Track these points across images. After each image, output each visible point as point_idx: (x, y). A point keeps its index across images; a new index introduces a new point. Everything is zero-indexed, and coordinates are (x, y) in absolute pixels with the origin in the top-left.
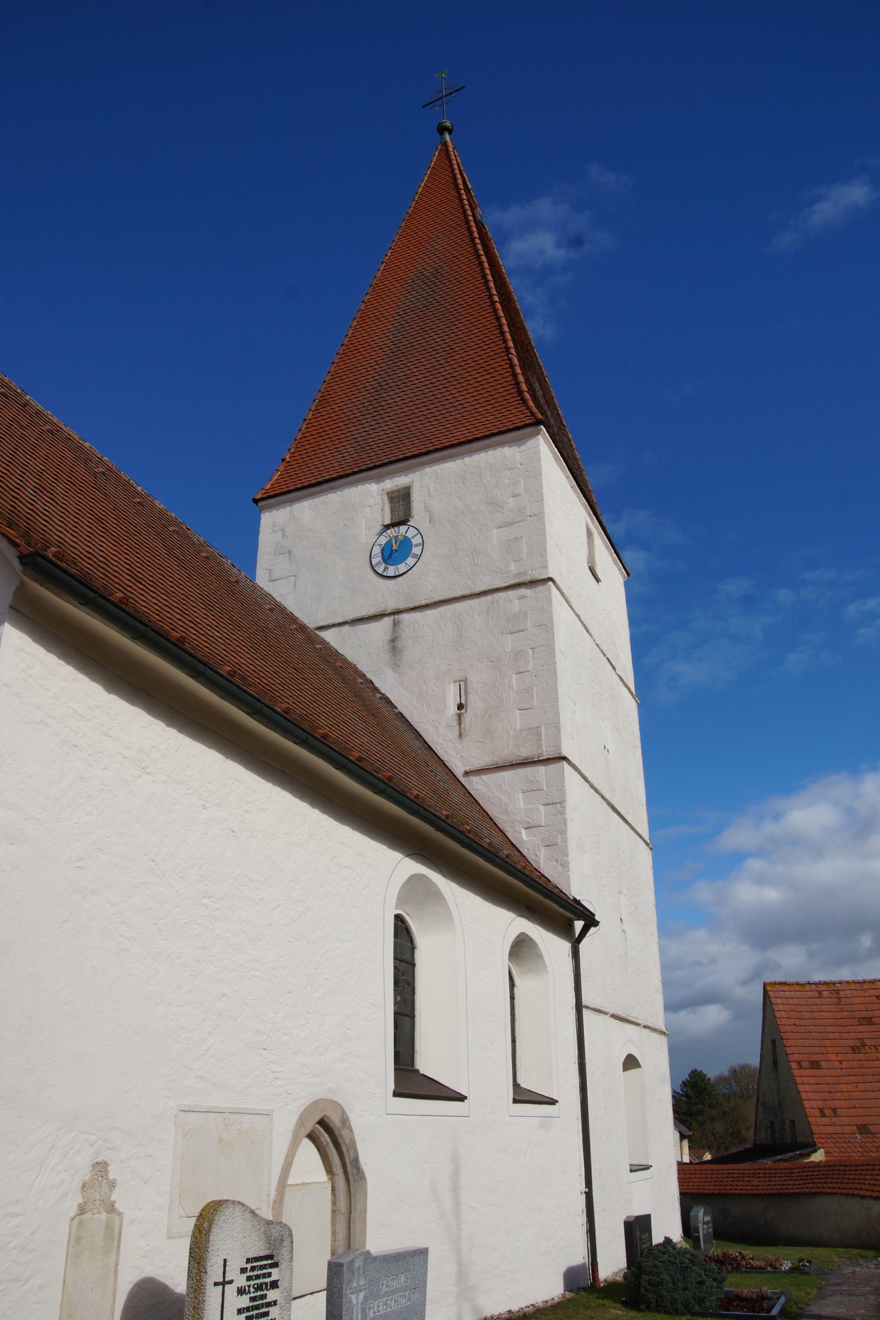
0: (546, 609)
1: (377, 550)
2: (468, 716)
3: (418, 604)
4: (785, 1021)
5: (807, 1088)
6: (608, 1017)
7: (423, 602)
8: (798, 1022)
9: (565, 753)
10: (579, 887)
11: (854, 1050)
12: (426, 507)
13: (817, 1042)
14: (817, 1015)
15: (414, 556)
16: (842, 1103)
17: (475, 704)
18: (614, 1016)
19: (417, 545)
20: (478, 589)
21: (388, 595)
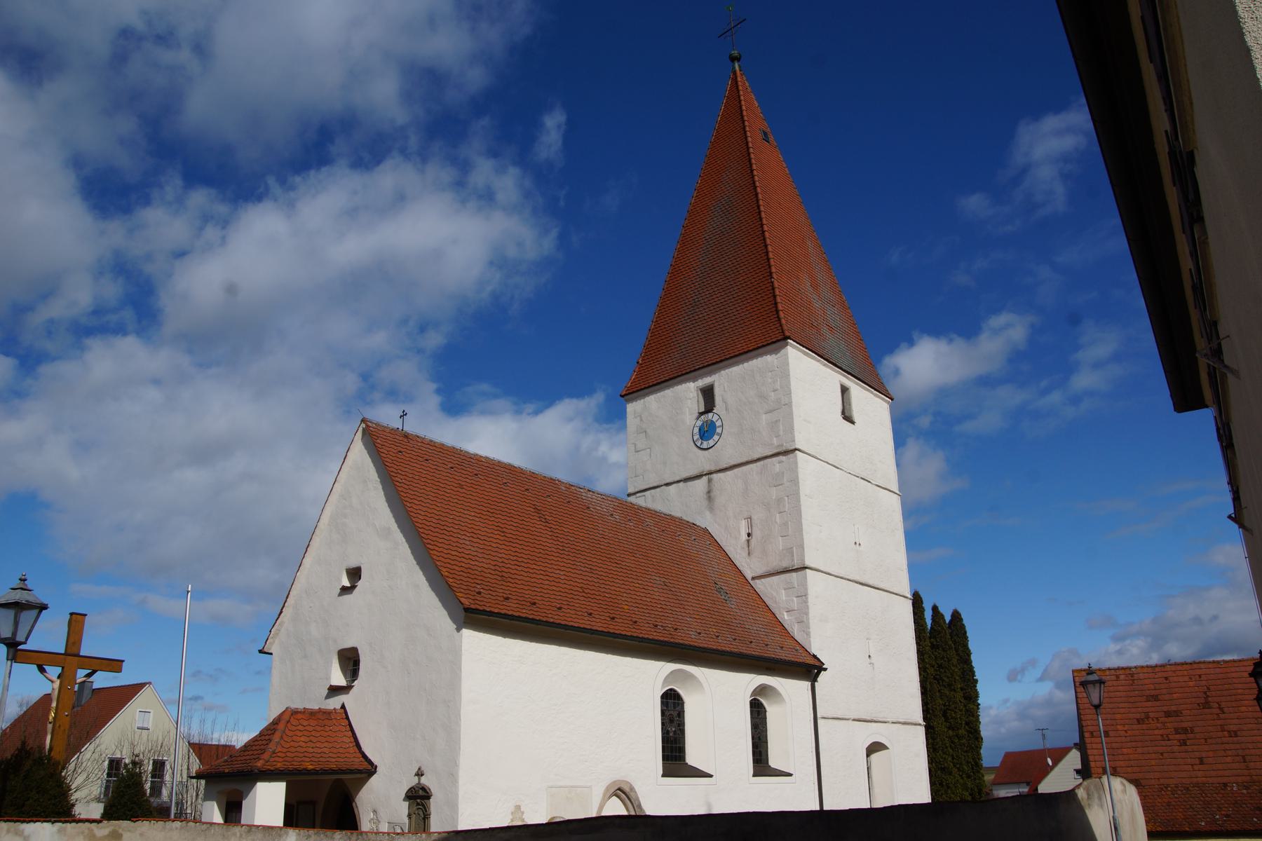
0: (794, 469)
1: (696, 430)
2: (753, 541)
9: (808, 563)
10: (818, 646)
11: (1139, 721)
17: (757, 534)
20: (756, 456)
21: (703, 461)
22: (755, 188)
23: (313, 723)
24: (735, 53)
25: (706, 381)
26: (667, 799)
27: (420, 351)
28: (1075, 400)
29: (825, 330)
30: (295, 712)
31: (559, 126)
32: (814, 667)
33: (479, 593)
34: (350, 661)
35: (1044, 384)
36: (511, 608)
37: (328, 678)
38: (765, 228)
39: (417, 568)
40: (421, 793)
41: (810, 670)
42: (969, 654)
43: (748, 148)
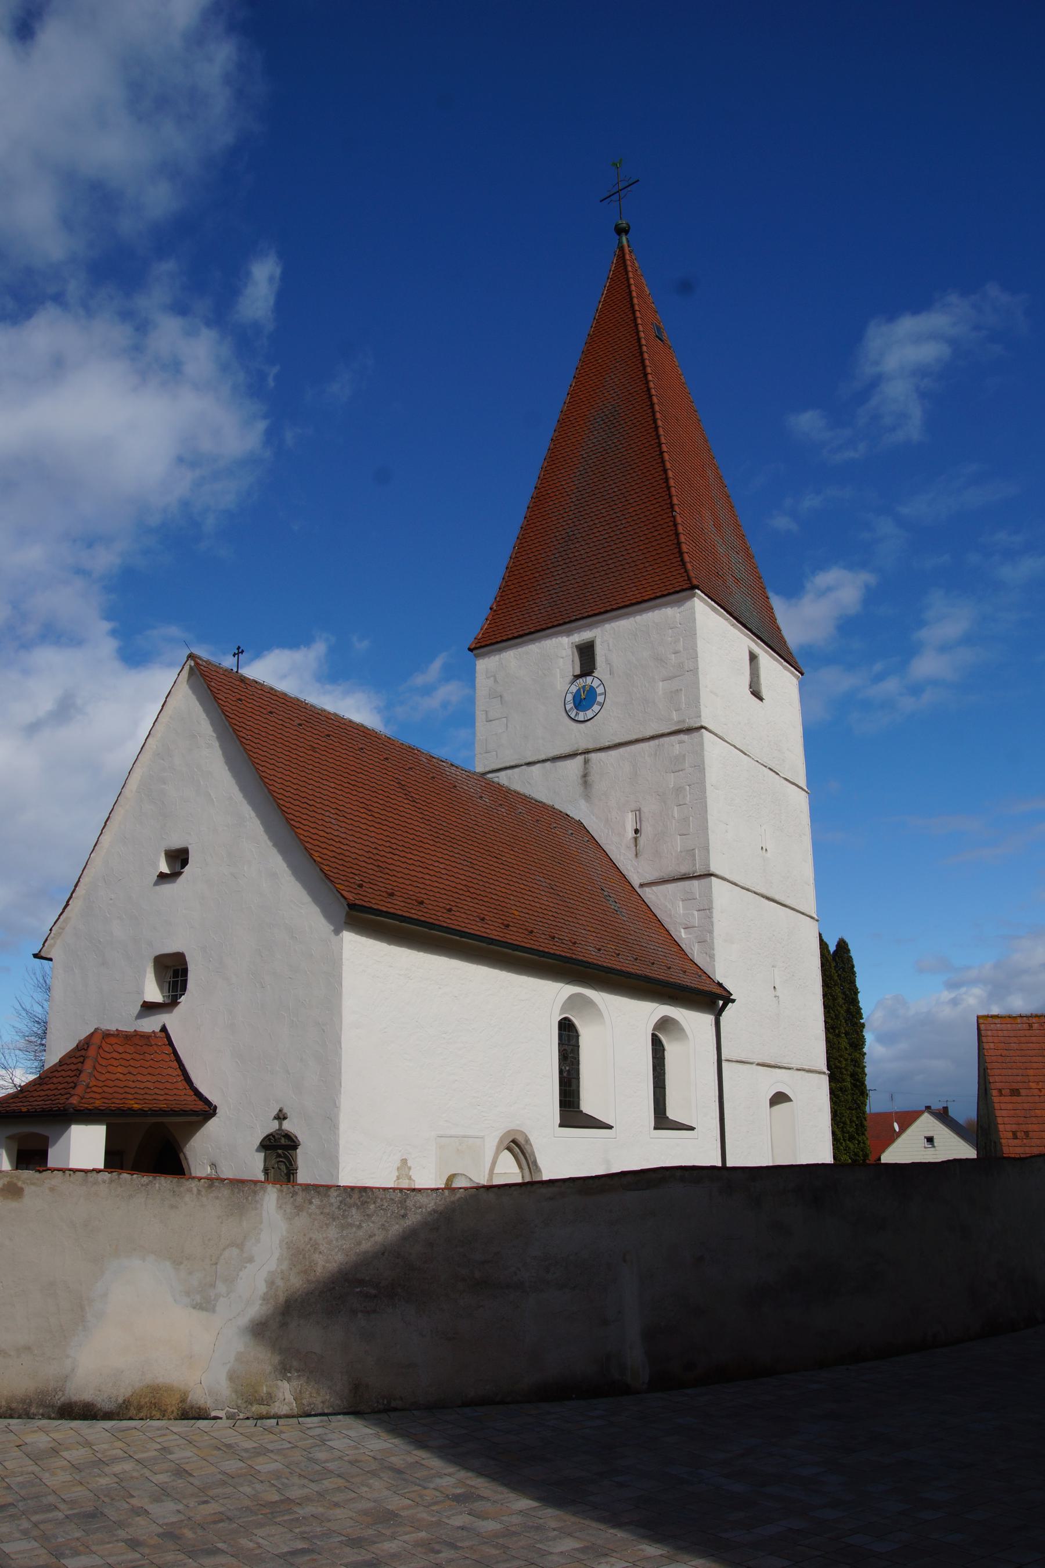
0: (699, 751)
1: (570, 697)
2: (642, 841)
3: (602, 745)
4: (992, 1052)
5: (1004, 1113)
6: (754, 1066)
7: (607, 744)
8: (1005, 1053)
9: (713, 869)
10: (725, 971)
12: (607, 660)
13: (1020, 1072)
14: (1024, 1046)
15: (599, 704)
16: (1035, 1127)
17: (647, 830)
18: (758, 1064)
19: (601, 694)
20: (649, 733)
21: (578, 736)
22: (650, 396)
23: (130, 1049)
24: (623, 223)
25: (585, 636)
26: (568, 1157)
27: (80, 571)
28: (916, 690)
29: (730, 581)
30: (107, 1035)
31: (271, 279)
32: (721, 997)
33: (361, 886)
34: (174, 972)
35: (878, 667)
36: (397, 906)
37: (140, 992)
38: (664, 448)
39: (274, 852)
40: (283, 1141)
41: (712, 999)
42: (856, 992)
43: (640, 346)
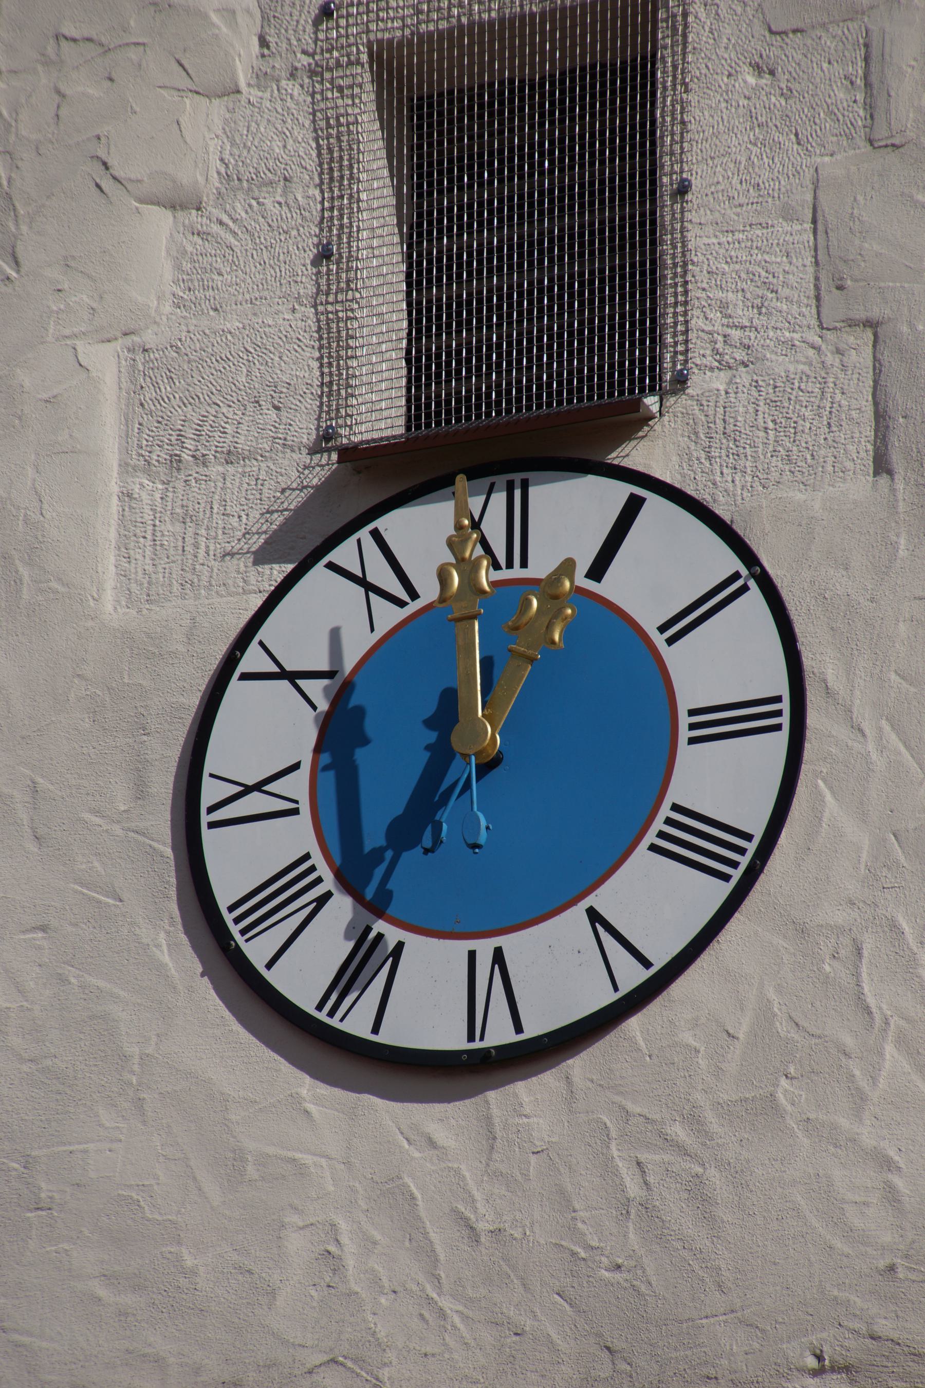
1: (267, 732)
15: (698, 841)
